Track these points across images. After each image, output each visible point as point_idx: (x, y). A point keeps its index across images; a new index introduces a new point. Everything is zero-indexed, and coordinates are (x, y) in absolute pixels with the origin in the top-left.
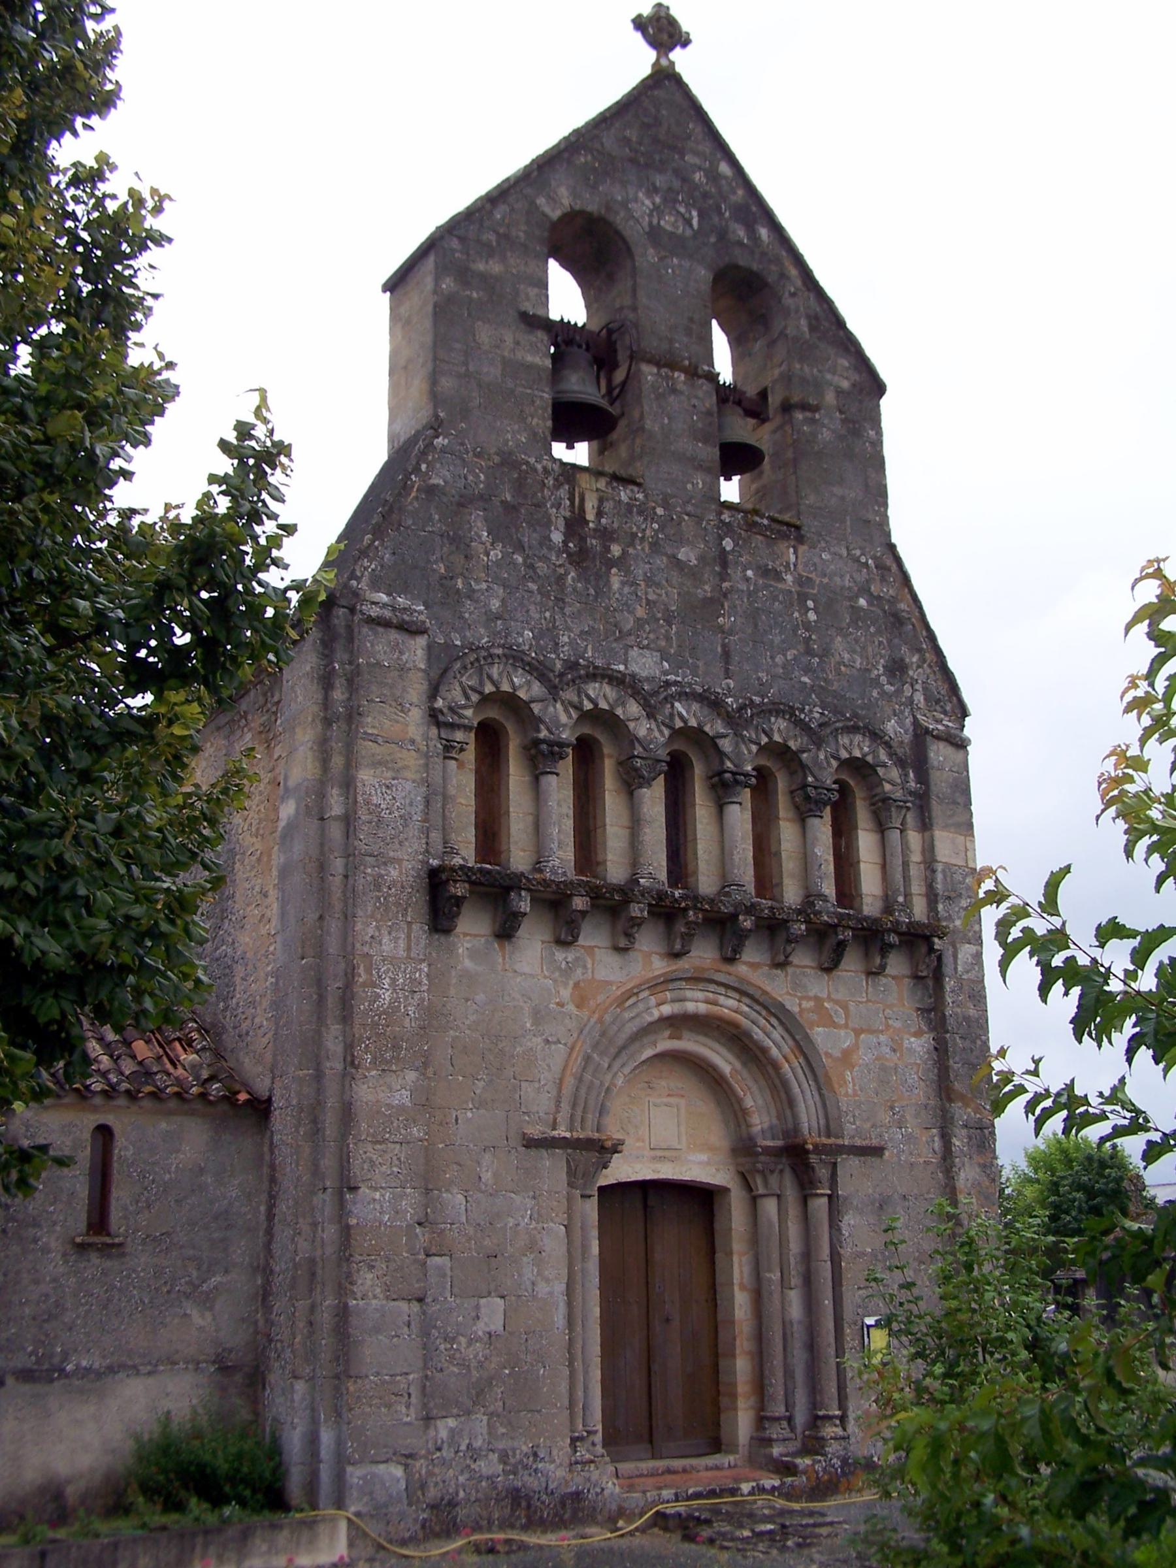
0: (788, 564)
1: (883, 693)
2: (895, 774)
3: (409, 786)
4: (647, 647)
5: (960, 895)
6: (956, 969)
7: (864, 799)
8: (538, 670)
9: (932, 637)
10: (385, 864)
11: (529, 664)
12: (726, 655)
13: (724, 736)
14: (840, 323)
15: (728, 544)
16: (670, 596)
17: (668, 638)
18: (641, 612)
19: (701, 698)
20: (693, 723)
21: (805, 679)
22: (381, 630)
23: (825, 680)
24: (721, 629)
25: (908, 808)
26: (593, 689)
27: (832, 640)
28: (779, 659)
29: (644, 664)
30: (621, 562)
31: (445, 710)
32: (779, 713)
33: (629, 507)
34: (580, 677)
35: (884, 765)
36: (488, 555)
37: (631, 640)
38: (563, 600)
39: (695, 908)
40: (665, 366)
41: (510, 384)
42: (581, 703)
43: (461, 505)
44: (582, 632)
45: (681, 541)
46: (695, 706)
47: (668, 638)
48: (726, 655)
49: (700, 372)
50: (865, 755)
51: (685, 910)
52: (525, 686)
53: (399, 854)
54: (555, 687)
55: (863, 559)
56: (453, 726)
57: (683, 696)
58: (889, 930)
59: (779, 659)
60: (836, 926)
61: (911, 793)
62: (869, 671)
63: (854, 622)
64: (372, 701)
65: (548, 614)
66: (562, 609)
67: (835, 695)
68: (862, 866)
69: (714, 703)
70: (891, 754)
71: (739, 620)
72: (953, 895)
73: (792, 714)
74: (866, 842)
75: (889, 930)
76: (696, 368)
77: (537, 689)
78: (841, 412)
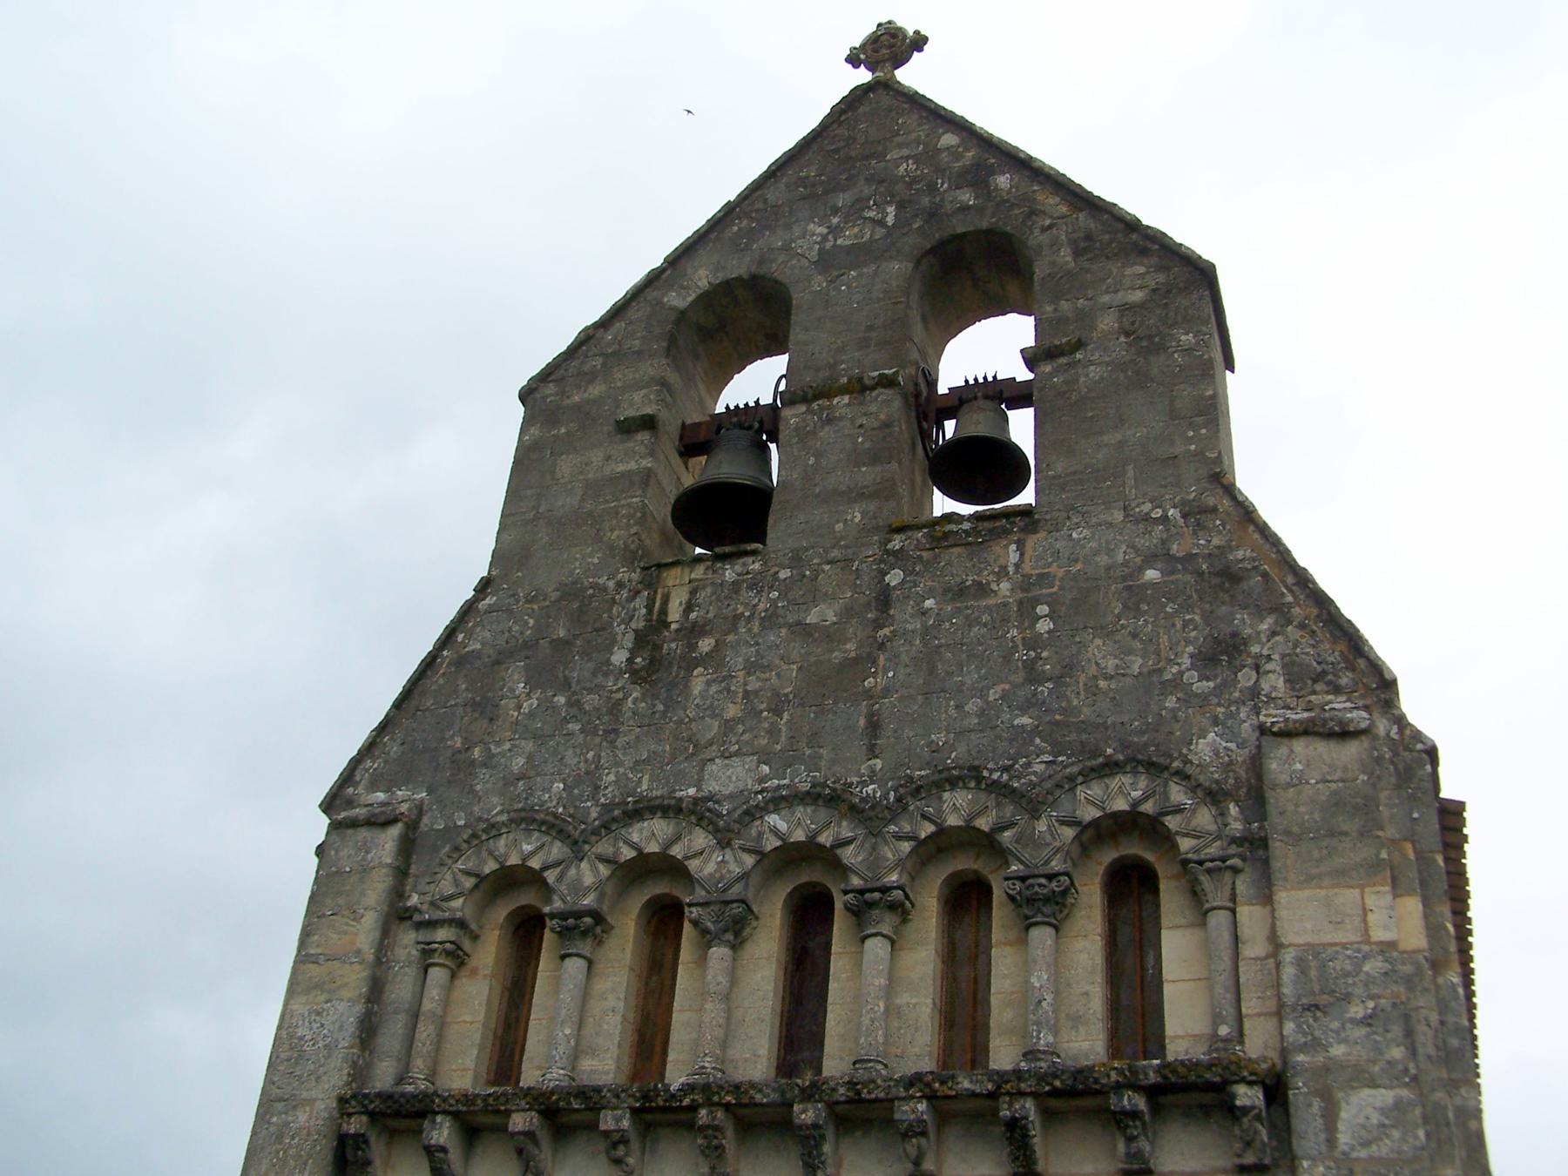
0: (1004, 568)
1: (1189, 698)
2: (1204, 818)
3: (342, 1007)
4: (736, 754)
5: (1347, 998)
6: (1331, 1142)
7: (1177, 877)
8: (554, 827)
9: (1303, 580)
10: (295, 1107)
11: (543, 822)
12: (874, 726)
13: (849, 842)
14: (1132, 225)
15: (894, 577)
16: (787, 677)
17: (773, 732)
18: (732, 711)
19: (811, 797)
20: (799, 836)
21: (1026, 720)
22: (350, 831)
23: (1064, 711)
24: (869, 695)
25: (1236, 871)
26: (637, 832)
27: (1083, 645)
28: (972, 706)
29: (728, 778)
30: (714, 659)
31: (425, 907)
32: (953, 783)
33: (736, 585)
34: (614, 820)
35: (1178, 810)
36: (519, 707)
37: (713, 751)
38: (615, 731)
39: (709, 1103)
40: (816, 397)
41: (588, 506)
42: (617, 853)
43: (498, 662)
44: (637, 763)
45: (814, 598)
46: (800, 812)
47: (773, 732)
48: (874, 726)
49: (867, 382)
50: (1136, 803)
51: (693, 1108)
52: (524, 849)
53: (313, 1094)
54: (576, 842)
55: (1158, 513)
56: (432, 924)
57: (778, 802)
58: (1118, 1087)
59: (972, 706)
60: (993, 1095)
61: (1234, 841)
62: (1160, 671)
63: (1132, 609)
64: (323, 915)
65: (590, 755)
66: (612, 742)
67: (1084, 726)
68: (1168, 989)
69: (831, 799)
70: (1194, 788)
71: (902, 671)
72: (1324, 999)
73: (979, 779)
74: (1178, 950)
75: (1118, 1087)
76: (860, 380)
77: (557, 850)
78: (1127, 335)
